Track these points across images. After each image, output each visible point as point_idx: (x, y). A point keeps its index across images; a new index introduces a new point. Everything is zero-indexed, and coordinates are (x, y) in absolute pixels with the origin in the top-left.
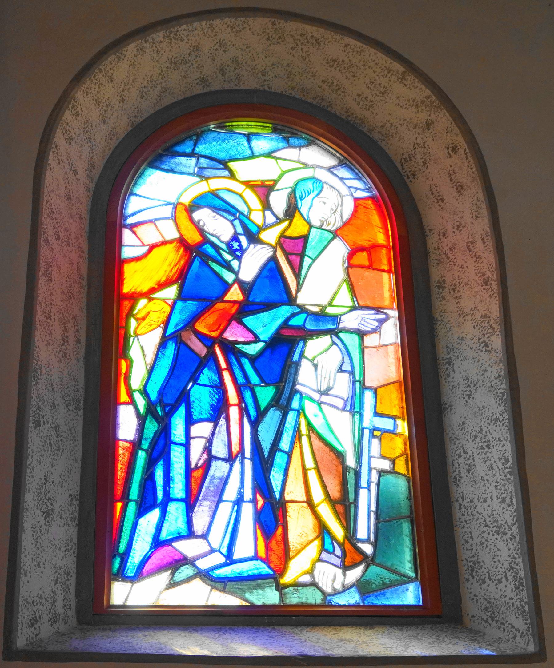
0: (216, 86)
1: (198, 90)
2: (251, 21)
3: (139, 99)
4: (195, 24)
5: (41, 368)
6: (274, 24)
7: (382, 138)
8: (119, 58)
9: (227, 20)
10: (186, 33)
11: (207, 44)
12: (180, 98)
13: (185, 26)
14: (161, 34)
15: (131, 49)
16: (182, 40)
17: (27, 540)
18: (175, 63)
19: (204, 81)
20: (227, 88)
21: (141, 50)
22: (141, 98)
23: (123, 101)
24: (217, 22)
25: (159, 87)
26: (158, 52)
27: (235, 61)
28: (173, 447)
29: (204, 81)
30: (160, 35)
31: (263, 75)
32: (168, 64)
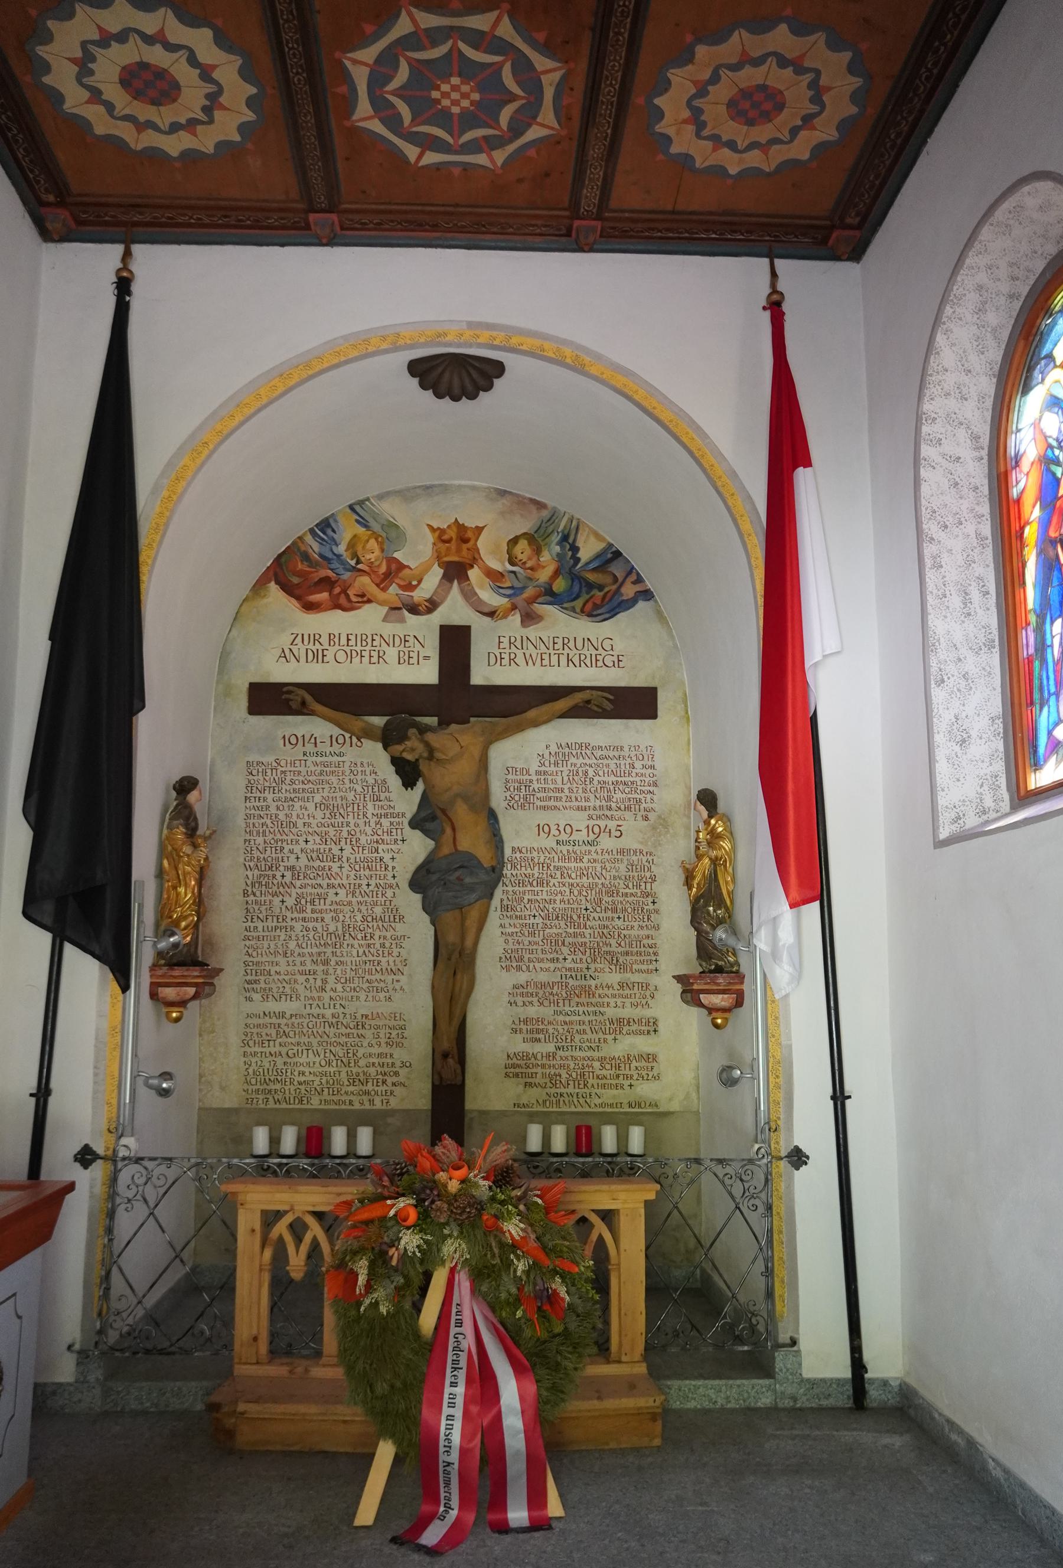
0: (1025, 290)
1: (1017, 305)
2: (981, 238)
3: (982, 356)
4: (959, 279)
5: (939, 640)
6: (992, 225)
7: (346, 865)
8: (938, 353)
9: (970, 254)
10: (961, 289)
11: (982, 277)
12: (1012, 322)
13: (955, 288)
14: (948, 308)
15: (940, 339)
16: (965, 295)
17: (942, 767)
18: (981, 310)
19: (1012, 296)
20: (1032, 283)
21: (946, 332)
22: (983, 353)
23: (970, 371)
24: (968, 261)
25: (988, 335)
26: (960, 319)
27: (1011, 265)
28: (119, 249)
29: (1012, 296)
30: (948, 310)
31: (1036, 253)
32: (976, 316)
